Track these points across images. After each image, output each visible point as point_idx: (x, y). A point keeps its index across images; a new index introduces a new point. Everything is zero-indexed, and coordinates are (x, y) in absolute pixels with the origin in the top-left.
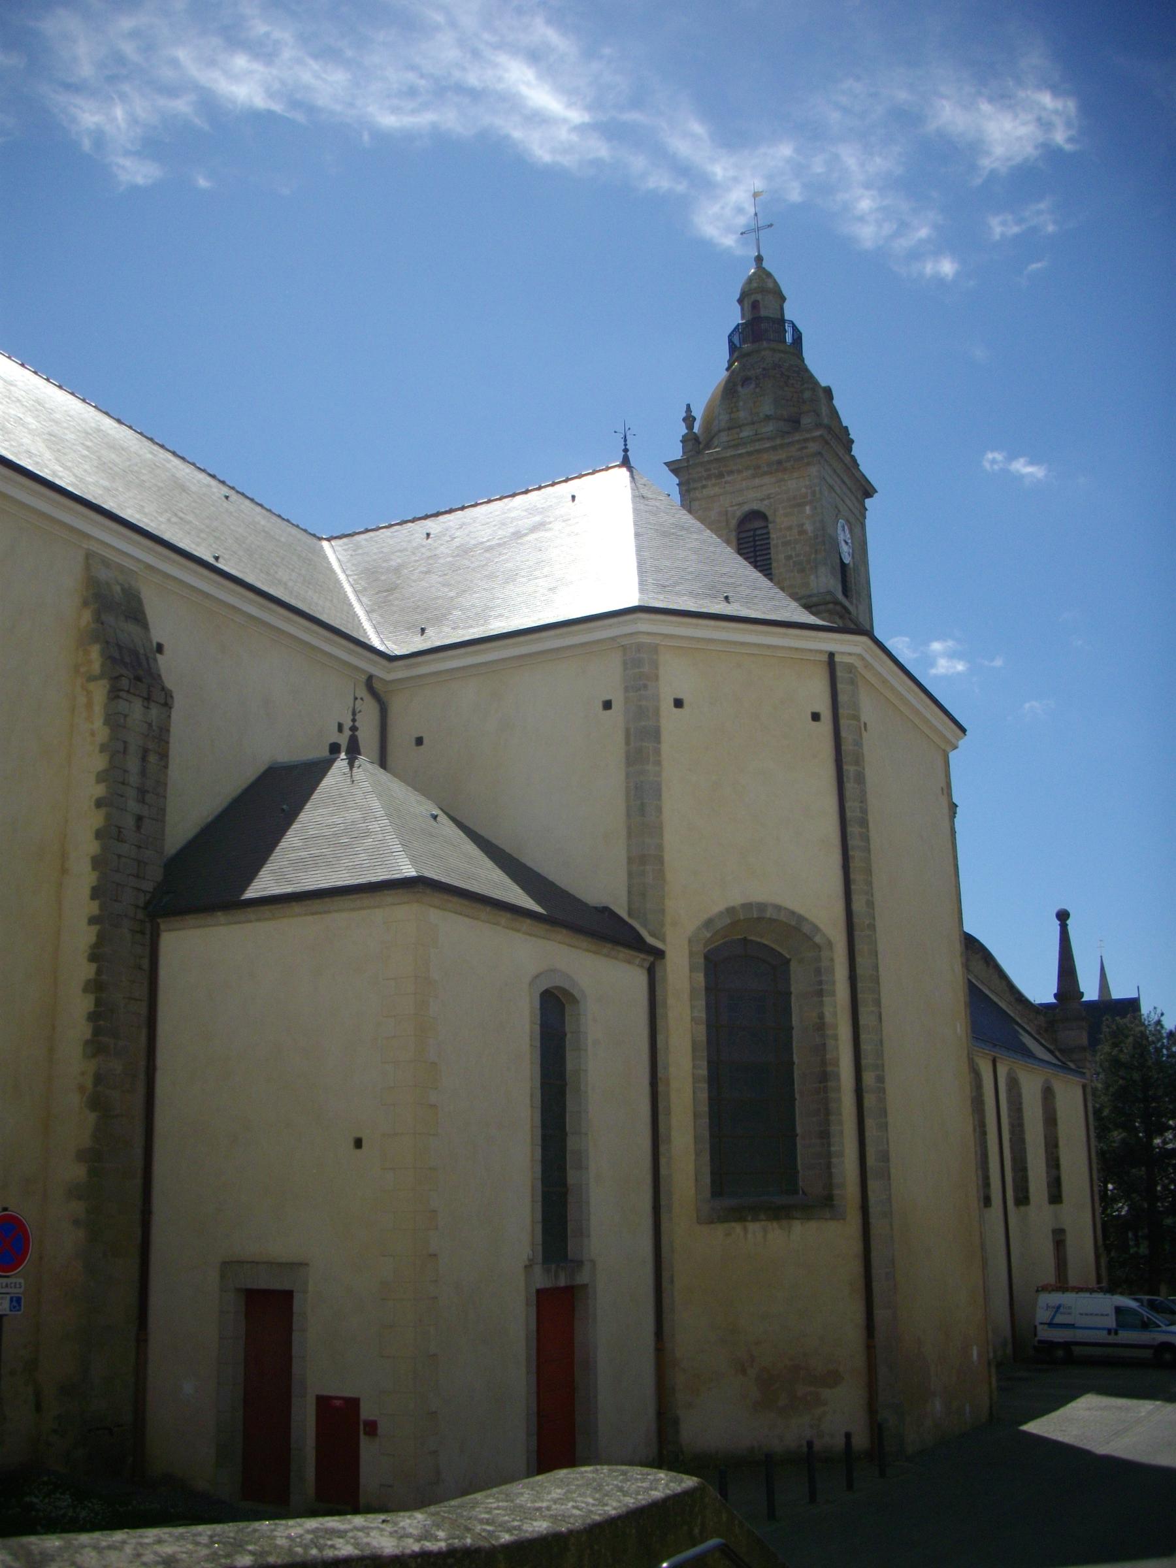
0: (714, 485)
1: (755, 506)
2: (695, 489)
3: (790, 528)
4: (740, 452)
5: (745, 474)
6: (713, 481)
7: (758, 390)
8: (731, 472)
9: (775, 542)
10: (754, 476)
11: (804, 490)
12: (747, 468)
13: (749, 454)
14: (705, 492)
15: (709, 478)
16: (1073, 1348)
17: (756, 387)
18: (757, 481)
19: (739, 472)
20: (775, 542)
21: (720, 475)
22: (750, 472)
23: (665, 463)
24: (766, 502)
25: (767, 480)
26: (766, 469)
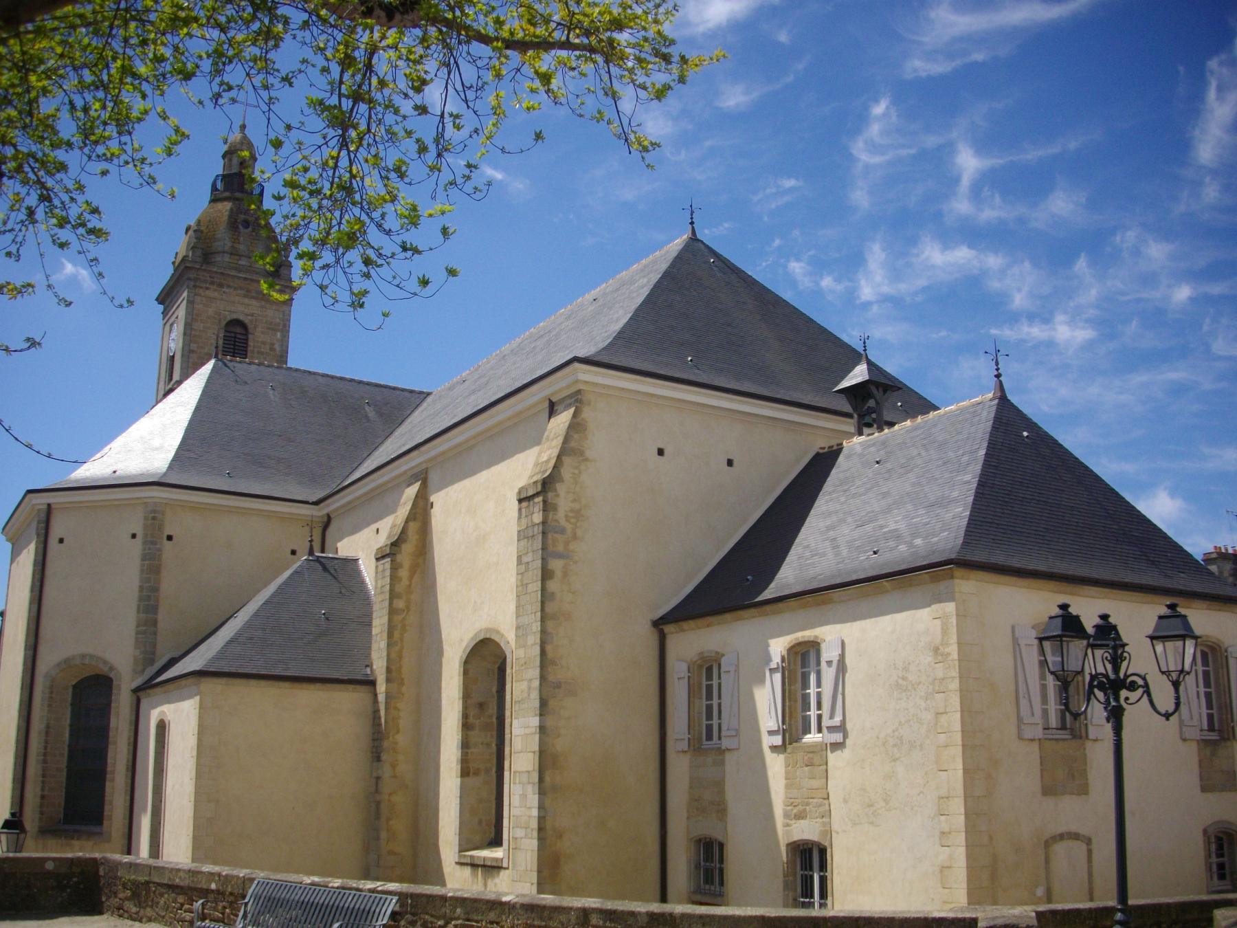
0: (215, 290)
1: (241, 318)
2: (201, 287)
3: (264, 343)
4: (241, 275)
5: (239, 292)
6: (215, 287)
7: (254, 234)
8: (229, 286)
9: (252, 348)
10: (245, 296)
11: (278, 320)
12: (241, 288)
13: (245, 279)
14: (207, 292)
15: (212, 283)
16: (1229, 887)
17: (253, 231)
18: (246, 301)
19: (235, 289)
20: (252, 348)
21: (221, 285)
22: (243, 292)
23: (429, 394)
24: (250, 318)
25: (254, 302)
26: (254, 294)
